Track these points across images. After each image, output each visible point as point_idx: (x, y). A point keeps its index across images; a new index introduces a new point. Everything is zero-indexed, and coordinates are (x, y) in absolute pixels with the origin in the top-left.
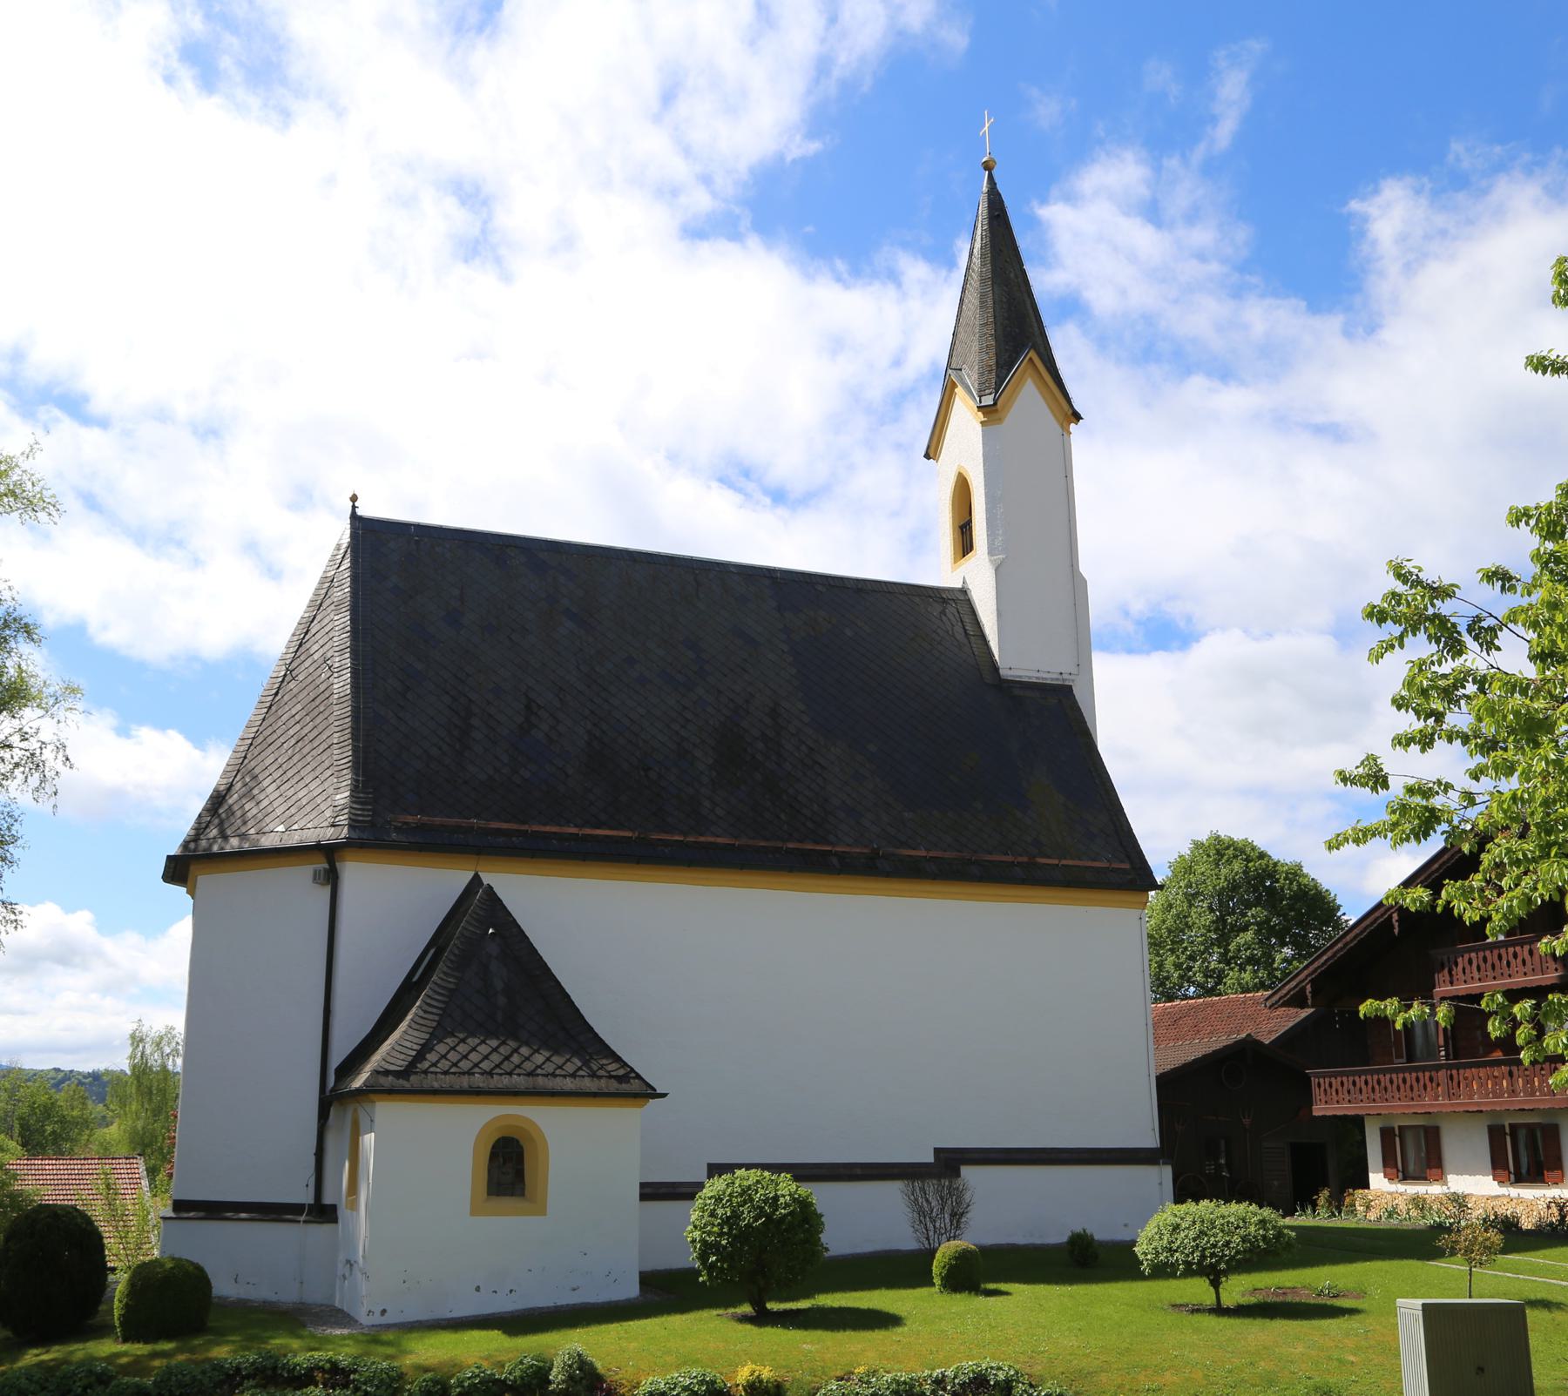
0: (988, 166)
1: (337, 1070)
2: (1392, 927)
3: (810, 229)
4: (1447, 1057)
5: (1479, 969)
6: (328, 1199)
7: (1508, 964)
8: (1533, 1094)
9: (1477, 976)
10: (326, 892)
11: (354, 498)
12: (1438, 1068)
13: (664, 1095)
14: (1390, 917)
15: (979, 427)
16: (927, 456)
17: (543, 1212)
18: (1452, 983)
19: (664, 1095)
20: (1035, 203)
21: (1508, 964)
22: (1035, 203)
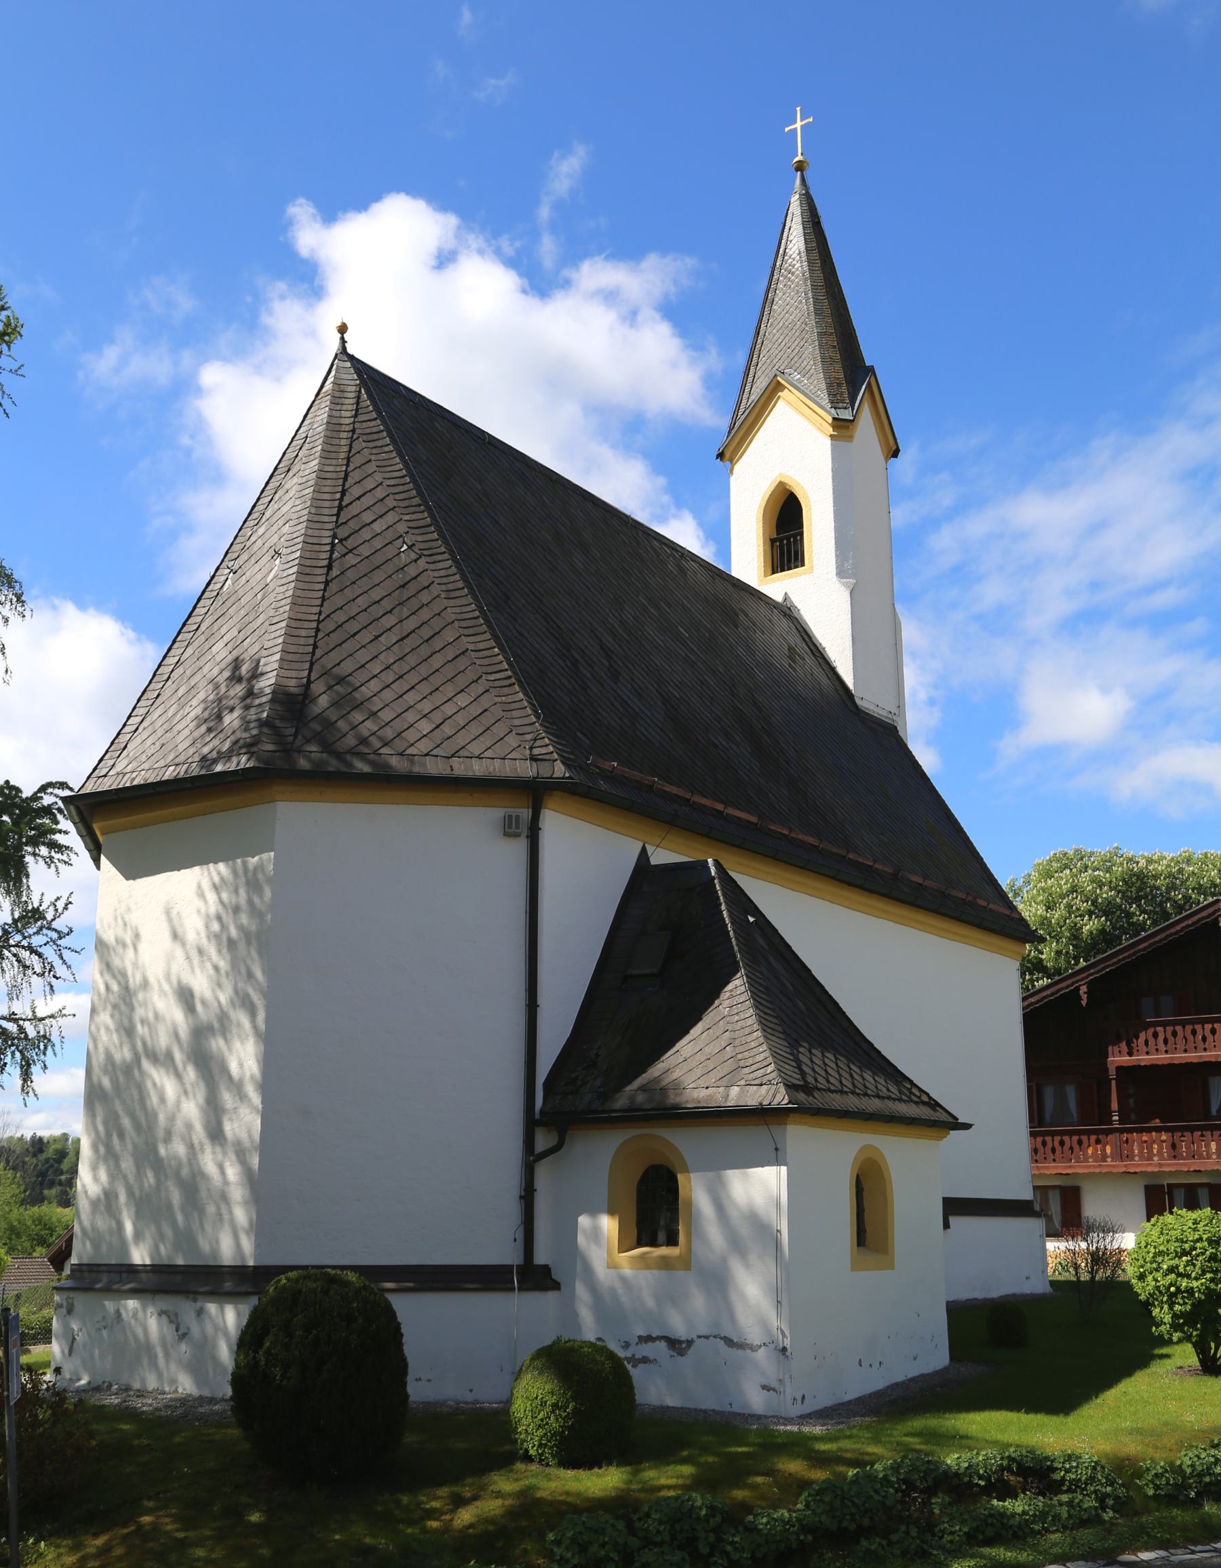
0: (800, 167)
1: (547, 1084)
2: (1080, 998)
3: (566, 170)
4: (1121, 1121)
5: (1166, 1041)
6: (540, 1258)
7: (1204, 1039)
8: (1150, 1158)
9: (1162, 1047)
10: (520, 847)
11: (343, 329)
12: (1108, 1132)
13: (967, 1126)
14: (1078, 989)
15: (828, 441)
16: (721, 456)
17: (891, 1266)
18: (1130, 1054)
19: (967, 1126)
20: (301, 211)
21: (1204, 1039)
22: (301, 211)
